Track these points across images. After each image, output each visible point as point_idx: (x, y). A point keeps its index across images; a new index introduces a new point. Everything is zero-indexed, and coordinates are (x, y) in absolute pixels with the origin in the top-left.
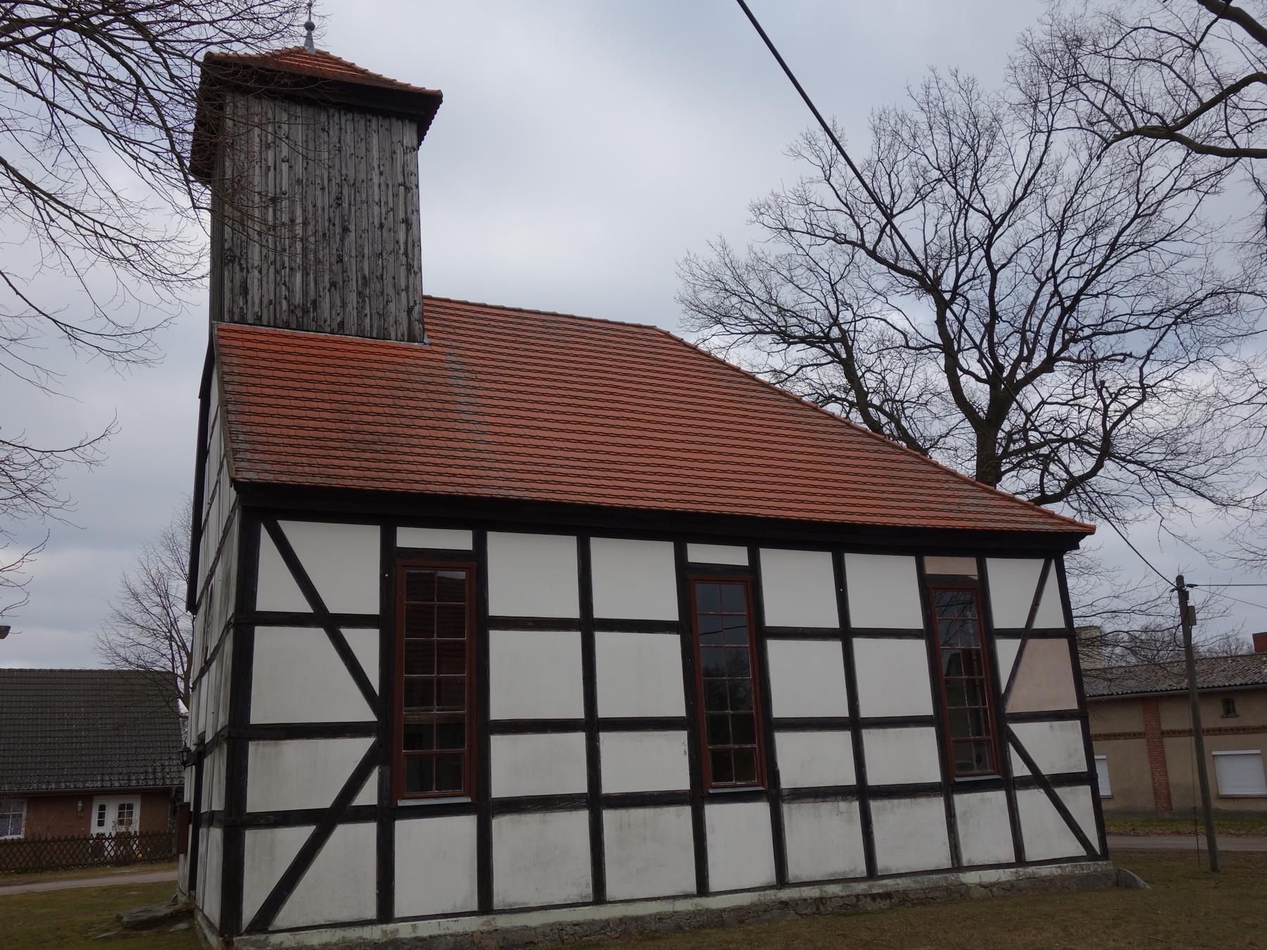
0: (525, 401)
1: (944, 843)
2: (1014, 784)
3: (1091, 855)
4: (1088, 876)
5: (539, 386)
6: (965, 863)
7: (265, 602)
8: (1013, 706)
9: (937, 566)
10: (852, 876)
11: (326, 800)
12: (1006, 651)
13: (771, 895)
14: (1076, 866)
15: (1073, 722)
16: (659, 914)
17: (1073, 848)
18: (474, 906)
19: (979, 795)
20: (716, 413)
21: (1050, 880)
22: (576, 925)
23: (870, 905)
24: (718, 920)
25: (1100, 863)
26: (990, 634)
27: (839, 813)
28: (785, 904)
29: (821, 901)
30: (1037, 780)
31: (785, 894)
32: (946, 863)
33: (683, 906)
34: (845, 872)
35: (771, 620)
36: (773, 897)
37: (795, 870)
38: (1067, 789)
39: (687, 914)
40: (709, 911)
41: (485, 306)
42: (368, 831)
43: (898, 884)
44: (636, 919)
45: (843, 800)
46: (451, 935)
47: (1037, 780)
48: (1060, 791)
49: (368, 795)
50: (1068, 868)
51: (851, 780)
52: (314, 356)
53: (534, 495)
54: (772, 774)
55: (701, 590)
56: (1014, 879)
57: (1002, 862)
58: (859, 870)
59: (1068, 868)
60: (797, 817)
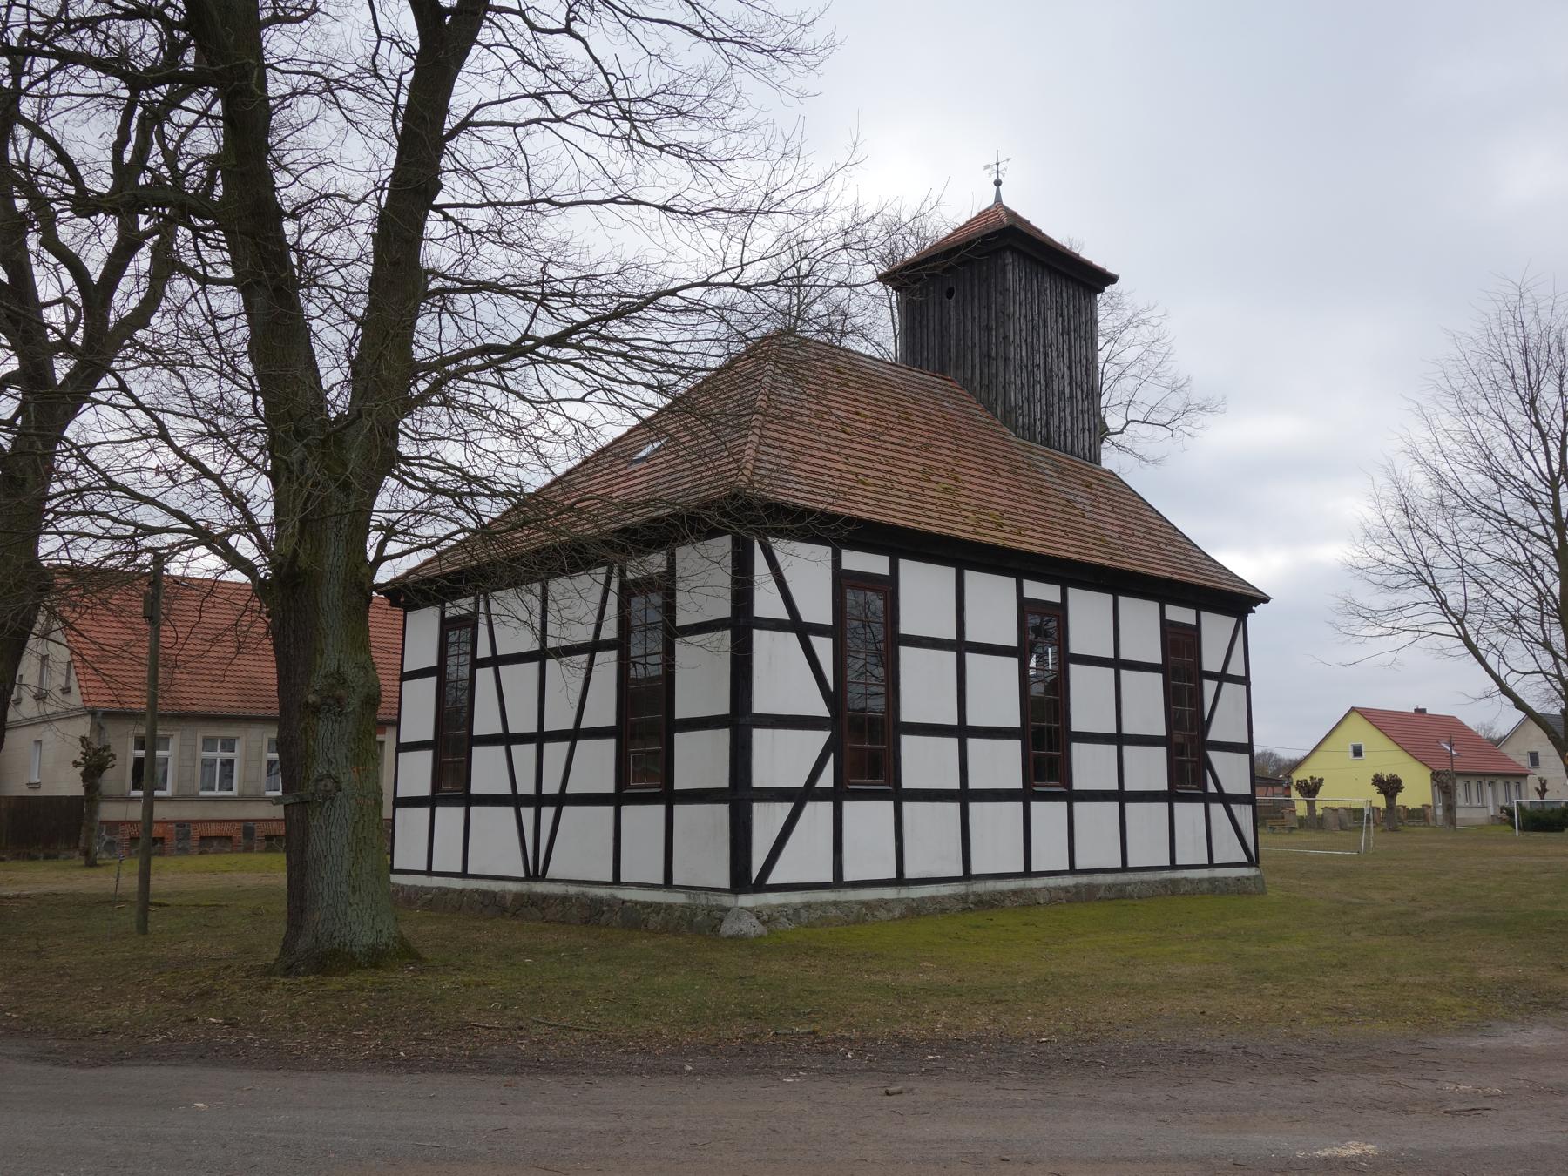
7: (759, 611)
8: (1214, 735)
9: (855, 561)
11: (800, 782)
12: (1209, 687)
35: (906, 628)
42: (826, 808)
49: (826, 780)
52: (988, 447)
54: (1066, 776)
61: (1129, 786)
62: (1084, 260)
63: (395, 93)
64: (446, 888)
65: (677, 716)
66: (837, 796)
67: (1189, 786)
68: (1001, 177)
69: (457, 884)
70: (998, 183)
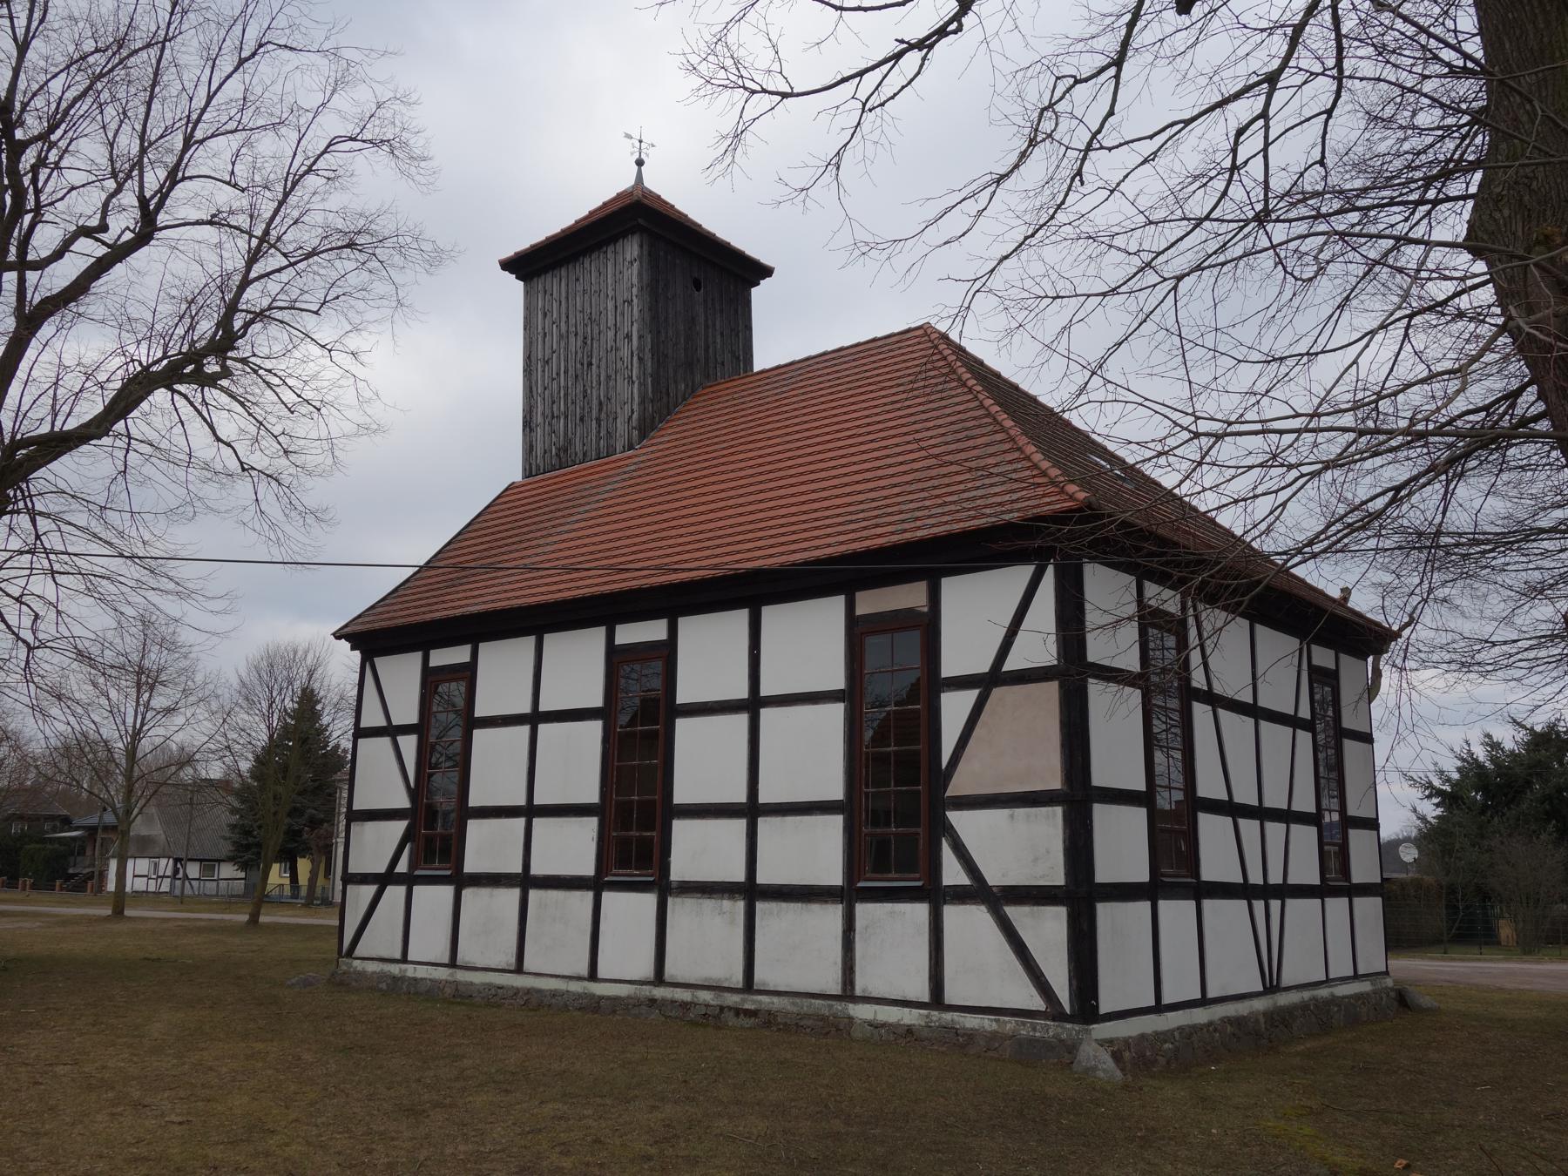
0: (799, 457)
1: (836, 963)
2: (944, 896)
3: (1054, 1011)
4: (1032, 1041)
5: (778, 444)
6: (858, 992)
10: (726, 985)
12: (955, 708)
13: (647, 991)
14: (1024, 1024)
15: (1050, 808)
16: (556, 990)
17: (1026, 997)
18: (446, 960)
19: (888, 906)
20: (705, 468)
21: (971, 1035)
22: (499, 988)
23: (729, 1017)
24: (595, 1005)
25: (1069, 1026)
26: (932, 684)
27: (722, 913)
28: (652, 1002)
29: (685, 1006)
30: (978, 891)
31: (659, 992)
32: (835, 988)
33: (575, 987)
34: (719, 980)
36: (648, 993)
37: (672, 970)
38: (1026, 909)
39: (574, 994)
40: (592, 996)
41: (825, 354)
43: (773, 1003)
44: (539, 991)
45: (729, 899)
46: (430, 980)
47: (978, 891)
48: (1011, 911)
49: (402, 867)
50: (1010, 1023)
51: (740, 876)
53: (868, 543)
55: (876, 646)
56: (923, 1024)
57: (908, 999)
58: (734, 980)
59: (1010, 1023)
60: (681, 911)
61: (537, 869)
62: (723, 241)
63: (359, 138)
64: (1188, 1026)
65: (471, 804)
66: (410, 881)
67: (890, 876)
68: (643, 156)
69: (1200, 1016)
70: (640, 163)
